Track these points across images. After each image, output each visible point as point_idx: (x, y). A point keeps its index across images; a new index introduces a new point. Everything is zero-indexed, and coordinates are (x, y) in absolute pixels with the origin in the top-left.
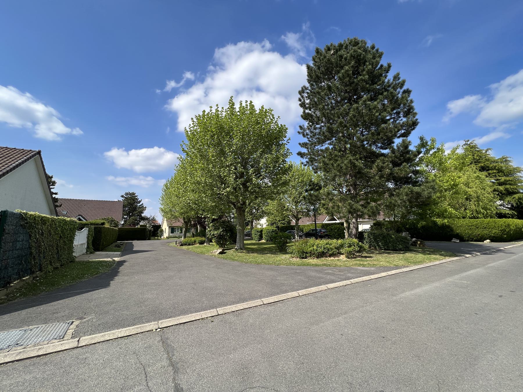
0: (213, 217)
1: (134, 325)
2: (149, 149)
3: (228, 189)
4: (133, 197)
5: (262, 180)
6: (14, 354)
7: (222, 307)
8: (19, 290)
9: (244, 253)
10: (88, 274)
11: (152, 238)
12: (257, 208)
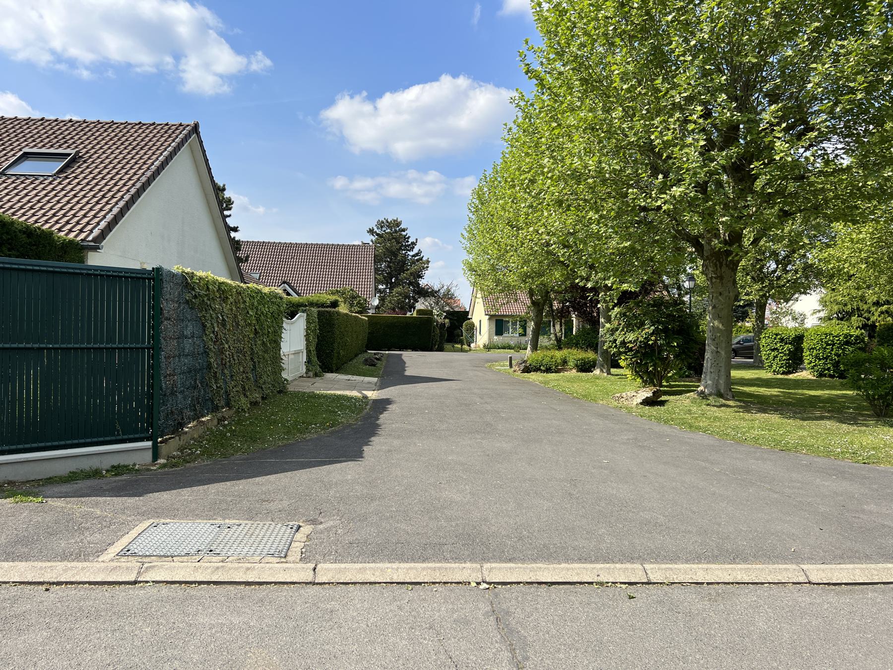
0: (625, 287)
1: (424, 561)
2: (428, 86)
3: (677, 191)
4: (396, 232)
5: (811, 145)
6: (207, 568)
7: (658, 563)
8: (199, 441)
9: (729, 410)
10: (315, 424)
11: (448, 346)
12: (784, 258)
